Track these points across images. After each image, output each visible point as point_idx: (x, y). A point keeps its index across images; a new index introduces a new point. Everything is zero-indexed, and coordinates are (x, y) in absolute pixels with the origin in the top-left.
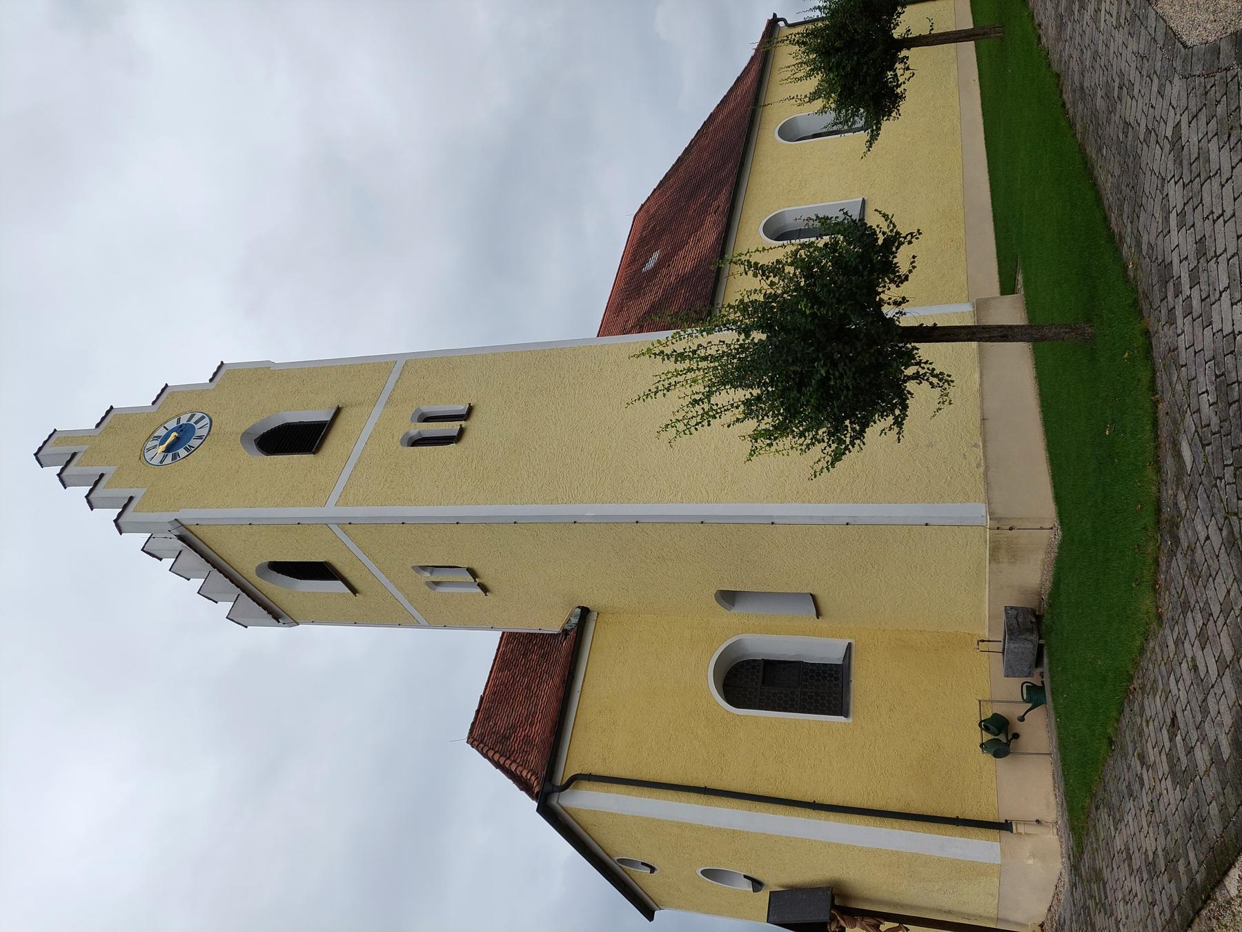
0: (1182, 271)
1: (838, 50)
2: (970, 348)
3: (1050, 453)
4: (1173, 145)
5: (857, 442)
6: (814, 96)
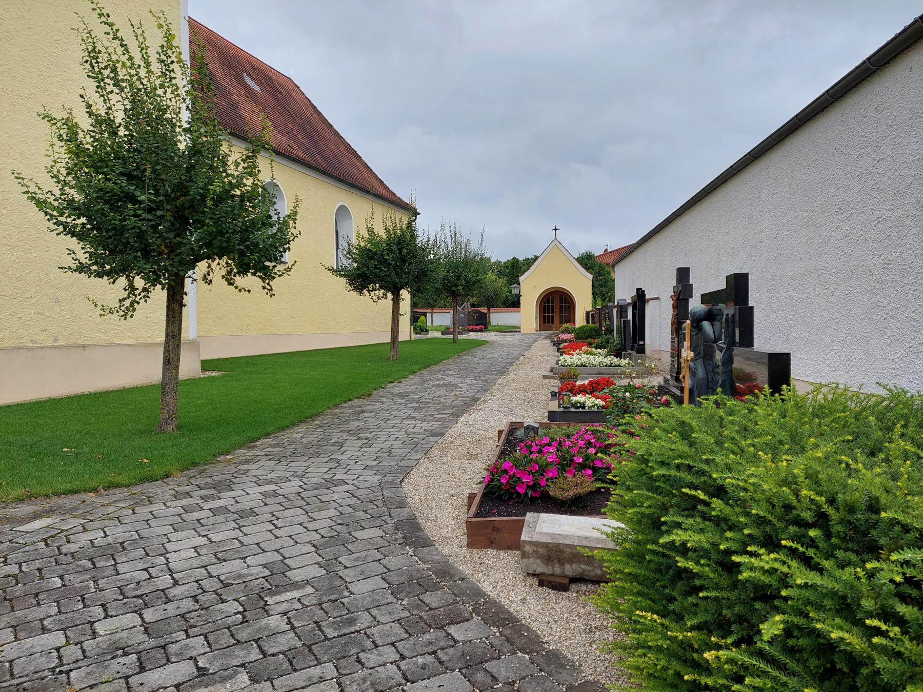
0: (225, 499)
1: (400, 251)
2: (160, 336)
3: (46, 401)
4: (330, 481)
5: (61, 228)
6: (370, 231)
